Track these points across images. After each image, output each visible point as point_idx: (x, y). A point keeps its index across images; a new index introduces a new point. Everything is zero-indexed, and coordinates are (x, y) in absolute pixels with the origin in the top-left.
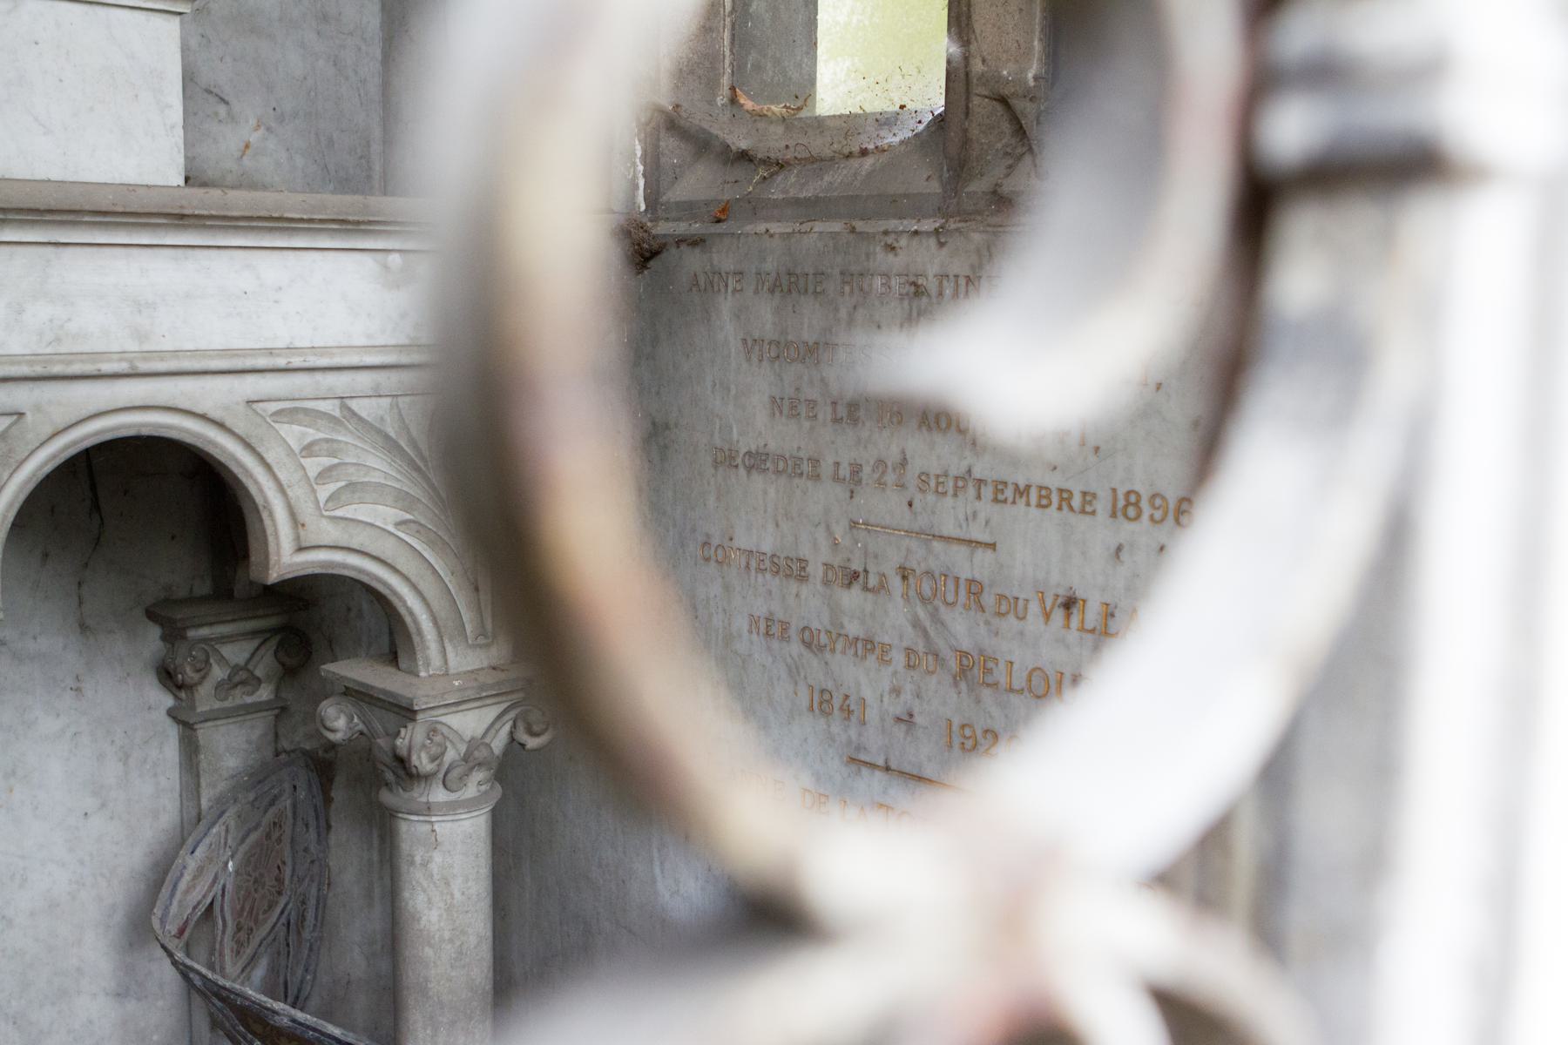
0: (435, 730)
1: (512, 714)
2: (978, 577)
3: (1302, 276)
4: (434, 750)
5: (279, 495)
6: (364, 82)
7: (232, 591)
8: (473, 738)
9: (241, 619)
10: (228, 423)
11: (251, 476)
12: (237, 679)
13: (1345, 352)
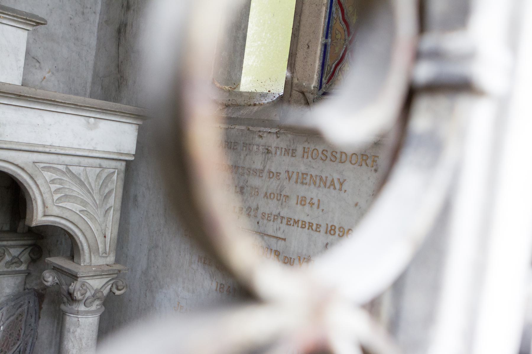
0: (84, 285)
1: (112, 282)
2: (278, 249)
3: (422, 120)
4: (83, 291)
5: (40, 196)
6: (88, 62)
7: (17, 229)
8: (97, 289)
9: (18, 240)
10: (26, 168)
11: (31, 188)
12: (14, 261)
13: (435, 145)
